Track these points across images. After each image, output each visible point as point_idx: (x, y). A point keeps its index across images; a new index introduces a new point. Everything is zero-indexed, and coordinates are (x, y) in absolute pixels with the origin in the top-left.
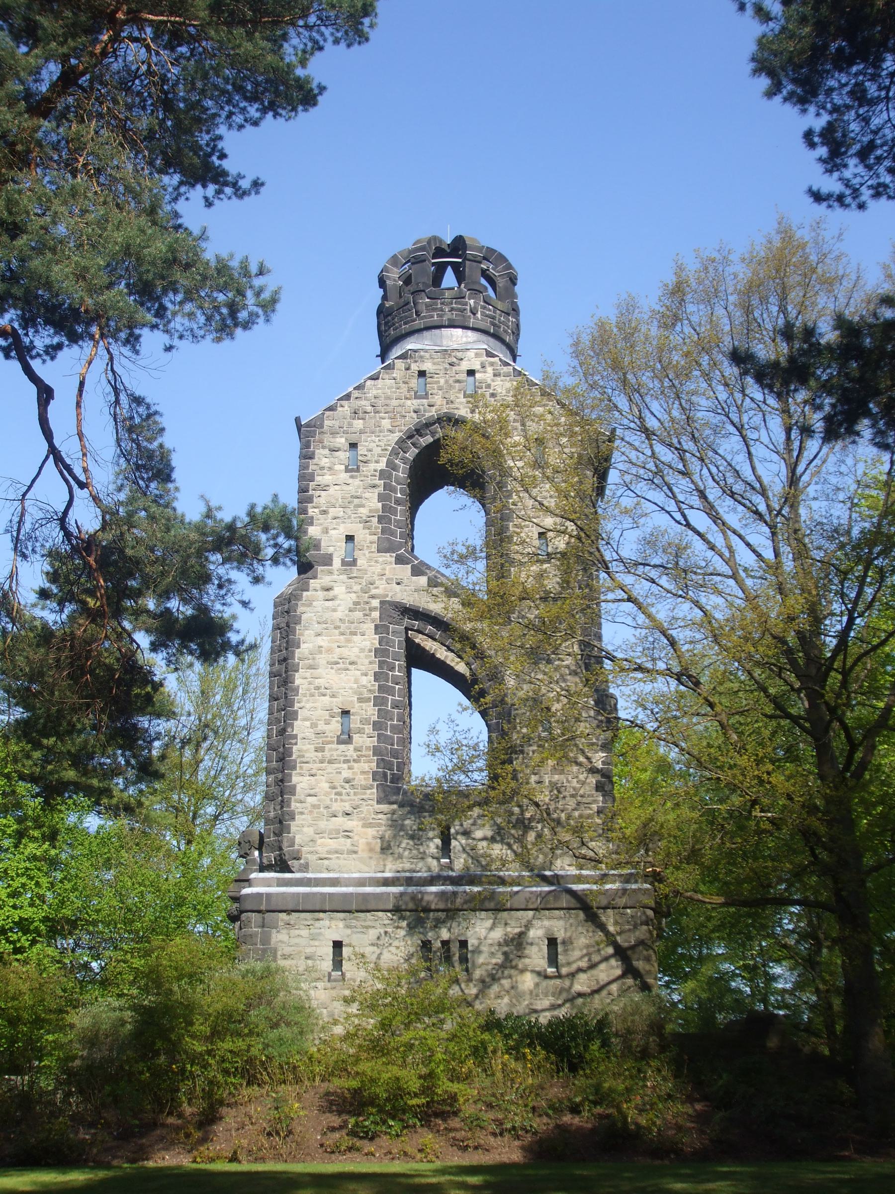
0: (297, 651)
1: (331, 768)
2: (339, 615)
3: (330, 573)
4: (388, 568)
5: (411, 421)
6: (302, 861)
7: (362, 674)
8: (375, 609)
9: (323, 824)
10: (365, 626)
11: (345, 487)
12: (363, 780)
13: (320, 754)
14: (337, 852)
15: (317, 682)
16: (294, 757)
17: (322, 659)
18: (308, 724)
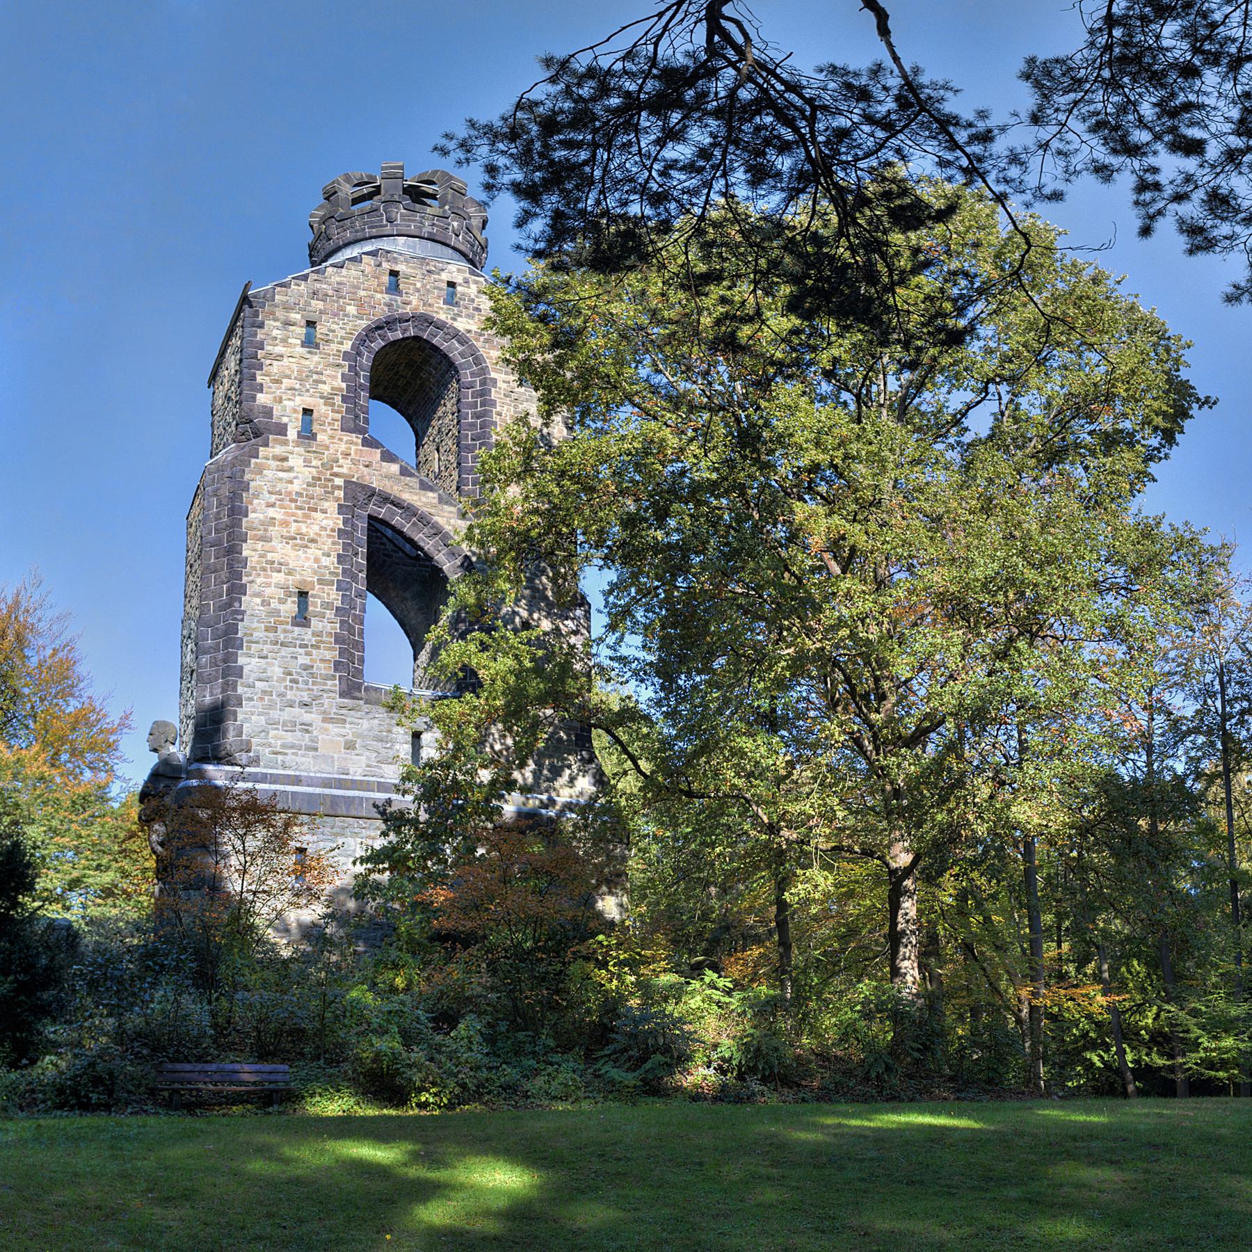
0: (244, 520)
1: (285, 651)
2: (296, 487)
3: (285, 443)
4: (353, 448)
5: (381, 313)
6: (251, 754)
7: (324, 554)
8: (339, 487)
9: (275, 714)
10: (326, 505)
11: (303, 361)
12: (323, 669)
13: (271, 635)
14: (292, 747)
15: (270, 556)
16: (240, 635)
17: (274, 531)
18: (258, 600)
